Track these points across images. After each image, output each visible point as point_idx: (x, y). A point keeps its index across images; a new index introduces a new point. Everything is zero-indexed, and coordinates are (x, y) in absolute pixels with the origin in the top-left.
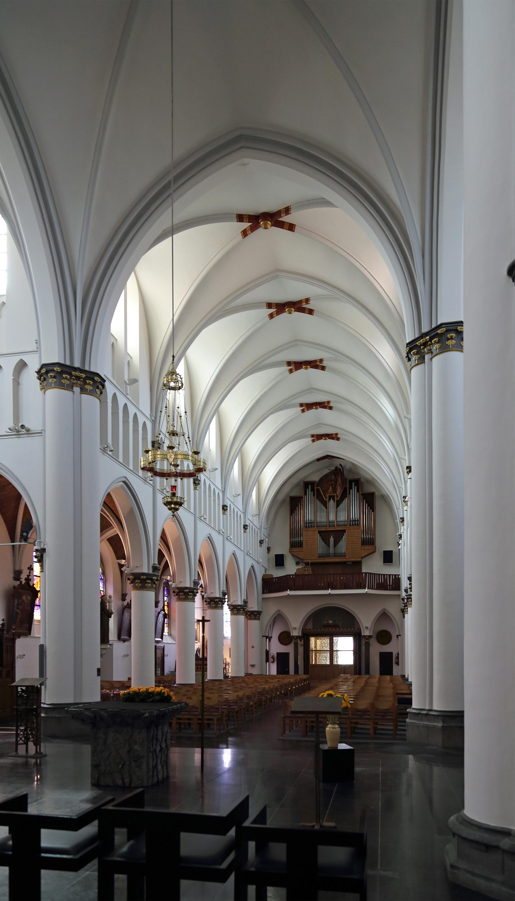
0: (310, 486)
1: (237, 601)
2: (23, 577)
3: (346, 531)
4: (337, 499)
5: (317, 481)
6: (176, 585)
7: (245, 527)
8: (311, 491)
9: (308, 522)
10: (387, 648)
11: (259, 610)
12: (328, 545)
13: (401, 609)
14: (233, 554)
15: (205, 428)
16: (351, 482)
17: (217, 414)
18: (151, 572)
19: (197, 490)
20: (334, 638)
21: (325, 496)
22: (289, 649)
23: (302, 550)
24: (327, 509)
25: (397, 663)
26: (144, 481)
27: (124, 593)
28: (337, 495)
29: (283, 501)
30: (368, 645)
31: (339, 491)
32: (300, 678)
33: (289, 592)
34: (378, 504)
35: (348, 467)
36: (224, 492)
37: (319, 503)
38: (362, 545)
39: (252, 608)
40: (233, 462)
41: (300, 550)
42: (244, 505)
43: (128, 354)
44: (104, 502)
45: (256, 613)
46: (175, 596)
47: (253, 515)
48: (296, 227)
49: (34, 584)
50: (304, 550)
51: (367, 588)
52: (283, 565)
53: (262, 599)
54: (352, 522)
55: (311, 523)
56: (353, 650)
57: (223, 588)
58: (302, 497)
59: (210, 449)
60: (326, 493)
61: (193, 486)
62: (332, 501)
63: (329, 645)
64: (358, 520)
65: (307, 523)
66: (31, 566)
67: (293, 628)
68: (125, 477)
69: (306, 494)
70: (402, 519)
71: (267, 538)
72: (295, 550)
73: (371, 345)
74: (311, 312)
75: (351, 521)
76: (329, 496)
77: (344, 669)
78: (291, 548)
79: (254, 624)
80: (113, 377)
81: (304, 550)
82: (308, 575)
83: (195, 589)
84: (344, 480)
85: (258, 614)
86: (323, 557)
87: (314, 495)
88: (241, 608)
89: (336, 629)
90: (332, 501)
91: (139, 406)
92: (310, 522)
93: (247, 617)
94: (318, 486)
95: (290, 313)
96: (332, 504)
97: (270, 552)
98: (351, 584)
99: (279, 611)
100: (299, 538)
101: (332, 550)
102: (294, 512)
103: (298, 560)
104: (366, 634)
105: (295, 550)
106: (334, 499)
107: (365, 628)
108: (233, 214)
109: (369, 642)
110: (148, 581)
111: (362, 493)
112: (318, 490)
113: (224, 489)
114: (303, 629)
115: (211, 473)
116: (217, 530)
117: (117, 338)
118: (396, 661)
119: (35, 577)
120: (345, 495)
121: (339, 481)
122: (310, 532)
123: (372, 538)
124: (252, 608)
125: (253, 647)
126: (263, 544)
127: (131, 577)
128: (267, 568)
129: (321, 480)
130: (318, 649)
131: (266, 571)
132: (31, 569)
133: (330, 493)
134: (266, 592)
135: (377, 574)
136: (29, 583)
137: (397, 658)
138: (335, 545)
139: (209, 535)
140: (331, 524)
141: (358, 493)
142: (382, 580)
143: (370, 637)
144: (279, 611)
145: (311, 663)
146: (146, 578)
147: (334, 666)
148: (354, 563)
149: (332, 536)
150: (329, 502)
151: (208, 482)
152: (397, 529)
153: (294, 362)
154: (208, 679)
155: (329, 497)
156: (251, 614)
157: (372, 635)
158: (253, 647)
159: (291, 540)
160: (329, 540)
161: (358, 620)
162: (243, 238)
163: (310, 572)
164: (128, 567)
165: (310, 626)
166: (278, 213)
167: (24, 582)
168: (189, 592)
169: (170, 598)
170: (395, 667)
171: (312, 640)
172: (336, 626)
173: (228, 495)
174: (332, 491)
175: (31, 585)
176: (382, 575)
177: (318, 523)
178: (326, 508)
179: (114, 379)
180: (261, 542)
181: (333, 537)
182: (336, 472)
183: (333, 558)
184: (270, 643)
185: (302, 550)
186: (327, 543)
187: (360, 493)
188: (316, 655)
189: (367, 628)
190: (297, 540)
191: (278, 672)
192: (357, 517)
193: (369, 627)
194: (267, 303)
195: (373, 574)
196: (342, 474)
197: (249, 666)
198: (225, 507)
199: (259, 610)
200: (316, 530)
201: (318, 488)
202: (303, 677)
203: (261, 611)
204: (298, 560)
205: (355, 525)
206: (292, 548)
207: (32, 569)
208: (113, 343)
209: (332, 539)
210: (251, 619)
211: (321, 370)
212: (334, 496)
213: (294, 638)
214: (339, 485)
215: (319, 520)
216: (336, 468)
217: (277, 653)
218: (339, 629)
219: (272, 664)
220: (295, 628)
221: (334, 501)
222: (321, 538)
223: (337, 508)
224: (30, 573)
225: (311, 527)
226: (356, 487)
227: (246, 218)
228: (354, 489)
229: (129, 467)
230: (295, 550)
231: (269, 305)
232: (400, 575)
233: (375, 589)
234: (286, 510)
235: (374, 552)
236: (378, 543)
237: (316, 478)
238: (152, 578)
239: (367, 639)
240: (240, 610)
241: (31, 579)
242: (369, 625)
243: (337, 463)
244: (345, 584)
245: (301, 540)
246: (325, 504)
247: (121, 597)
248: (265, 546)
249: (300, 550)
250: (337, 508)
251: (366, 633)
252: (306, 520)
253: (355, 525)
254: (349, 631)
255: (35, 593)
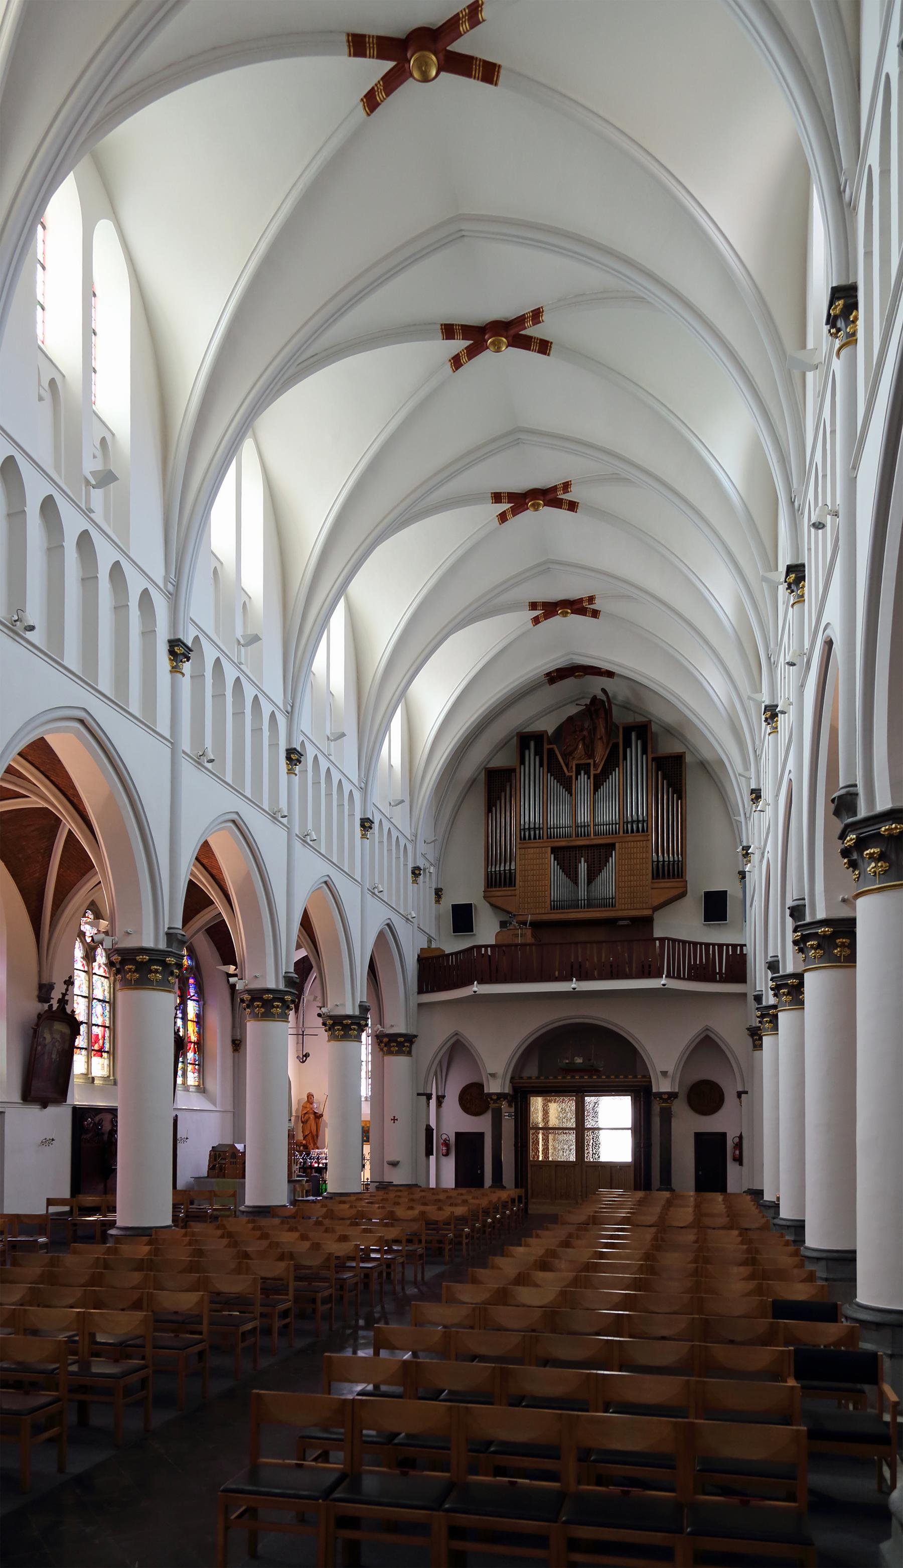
0: (532, 744)
1: (343, 1005)
2: (56, 995)
3: (617, 845)
4: (596, 772)
5: (550, 732)
6: (247, 985)
7: (366, 824)
8: (535, 755)
9: (527, 826)
10: (712, 1124)
11: (409, 1032)
12: (575, 882)
13: (748, 1029)
14: (388, 925)
15: (384, 726)
16: (628, 730)
17: (403, 700)
18: (162, 945)
19: (368, 839)
20: (586, 1098)
21: (567, 765)
22: (481, 1124)
23: (513, 893)
24: (571, 795)
25: (739, 1160)
26: (196, 765)
27: (44, 982)
28: (594, 762)
29: (473, 782)
30: (667, 1117)
31: (601, 754)
32: (490, 1202)
33: (477, 988)
34: (693, 783)
35: (620, 698)
36: (290, 715)
37: (553, 782)
38: (653, 878)
39: (392, 1026)
40: (314, 636)
41: (509, 893)
42: (413, 826)
43: (242, 589)
44: (197, 859)
45: (402, 1039)
46: (326, 1031)
47: (392, 804)
48: (503, 72)
49: (73, 1012)
50: (517, 892)
51: (666, 977)
52: (471, 929)
53: (416, 1005)
54: (629, 826)
55: (535, 828)
56: (630, 1126)
57: (362, 993)
58: (514, 770)
59: (392, 763)
60: (571, 758)
61: (285, 765)
62: (583, 777)
63: (574, 1116)
64: (643, 821)
65: (524, 829)
66: (71, 977)
67: (489, 1074)
68: (237, 813)
69: (522, 762)
70: (756, 794)
71: (432, 865)
72: (499, 894)
73: (679, 188)
74: (572, 506)
75: (627, 822)
76: (577, 765)
77: (611, 1173)
78: (488, 887)
79: (399, 1064)
80: (107, 518)
81: (517, 892)
82: (523, 945)
83: (169, 954)
84: (611, 728)
85: (406, 1041)
86: (563, 908)
87: (541, 765)
88: (352, 1024)
89: (590, 1077)
90: (583, 777)
91: (129, 551)
92: (537, 826)
93: (382, 1050)
94: (550, 743)
95: (536, 510)
96: (583, 783)
97: (443, 901)
98: (627, 970)
99: (457, 1034)
100: (508, 864)
101: (582, 893)
102: (496, 803)
103: (505, 918)
104: (662, 1090)
105: (499, 894)
106: (587, 773)
107: (659, 1074)
108: (435, 324)
109: (670, 1108)
110: (277, 1003)
111: (653, 755)
112: (551, 752)
113: (292, 707)
114: (512, 1078)
115: (332, 744)
116: (267, 809)
117: (114, 432)
118: (734, 1153)
119: (75, 997)
120: (612, 762)
121: (602, 730)
122: (532, 851)
123: (678, 861)
124: (392, 1026)
125: (394, 1120)
126: (371, 831)
127: (246, 997)
128: (432, 935)
129: (559, 730)
130: (551, 1124)
131: (430, 941)
132: (70, 982)
133: (580, 758)
134: (427, 988)
135: (690, 943)
136: (65, 1009)
137: (739, 1145)
138: (591, 879)
139: (388, 921)
140: (580, 830)
141: (644, 757)
142: (701, 958)
143: (672, 1096)
144: (457, 1034)
145: (531, 1159)
146: (150, 960)
147: (587, 1166)
148: (634, 920)
149: (583, 859)
150: (577, 779)
151: (324, 764)
152: (734, 829)
153: (462, 326)
154: (247, 1203)
155: (576, 768)
156: (390, 1042)
157: (677, 1090)
158: (394, 1120)
159: (489, 870)
160: (577, 868)
161: (643, 1055)
162: (500, 524)
163: (529, 939)
164: (242, 979)
165: (531, 1071)
166: (520, 321)
167: (55, 1007)
168: (275, 999)
169: (204, 1004)
170: (732, 1168)
171: (537, 1103)
172: (592, 1070)
173: (305, 722)
174: (583, 753)
175: (69, 1011)
176: (701, 944)
177: (550, 828)
178: (570, 793)
179: (59, 473)
180: (416, 872)
181: (585, 862)
182: (593, 709)
183: (586, 910)
184: (441, 1109)
185: (513, 893)
186: (572, 875)
187: (650, 756)
188: (546, 1140)
189: (664, 1074)
190: (502, 869)
191: (460, 1181)
192: (642, 813)
193: (671, 1072)
194: (348, 35)
195: (679, 941)
196: (608, 712)
197: (385, 1164)
198: (293, 753)
199: (412, 1031)
200: (546, 844)
201: (551, 746)
202: (499, 1198)
203: (416, 1034)
204: (505, 918)
205: (638, 831)
206: (489, 889)
207: (73, 983)
208: (245, 603)
209: (583, 867)
210: (390, 1053)
211: (539, 352)
212: (589, 764)
213: (492, 1099)
214: (601, 738)
215: (552, 822)
216: (594, 699)
217: (456, 1133)
218: (599, 1077)
219: (444, 1160)
220: (493, 1075)
221: (589, 778)
222: (558, 864)
223: (594, 794)
224: (67, 990)
225: (535, 838)
226: (639, 742)
227: (369, 43)
228: (636, 746)
229: (97, 686)
230: (498, 892)
231: (533, 606)
232: (745, 945)
233: (684, 979)
234: (478, 800)
235: (683, 894)
236: (690, 875)
237: (548, 725)
238: (165, 961)
239: (665, 1101)
240: (351, 1029)
241: (67, 1001)
242: (670, 1068)
243: (596, 685)
244: (611, 966)
245: (510, 869)
246: (567, 785)
247: (35, 993)
248: (427, 884)
249: (509, 893)
250: (594, 794)
251: (663, 1086)
252: (522, 822)
253: (638, 831)
254: (621, 1082)
255: (74, 1026)
